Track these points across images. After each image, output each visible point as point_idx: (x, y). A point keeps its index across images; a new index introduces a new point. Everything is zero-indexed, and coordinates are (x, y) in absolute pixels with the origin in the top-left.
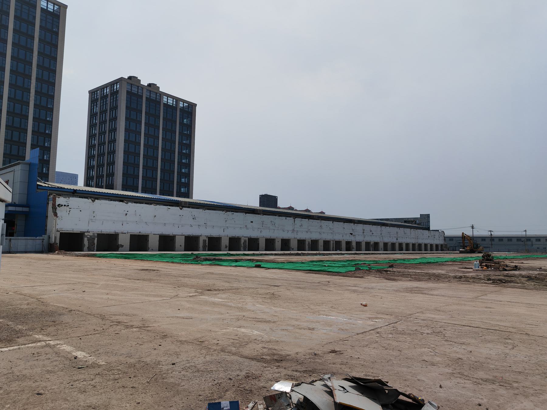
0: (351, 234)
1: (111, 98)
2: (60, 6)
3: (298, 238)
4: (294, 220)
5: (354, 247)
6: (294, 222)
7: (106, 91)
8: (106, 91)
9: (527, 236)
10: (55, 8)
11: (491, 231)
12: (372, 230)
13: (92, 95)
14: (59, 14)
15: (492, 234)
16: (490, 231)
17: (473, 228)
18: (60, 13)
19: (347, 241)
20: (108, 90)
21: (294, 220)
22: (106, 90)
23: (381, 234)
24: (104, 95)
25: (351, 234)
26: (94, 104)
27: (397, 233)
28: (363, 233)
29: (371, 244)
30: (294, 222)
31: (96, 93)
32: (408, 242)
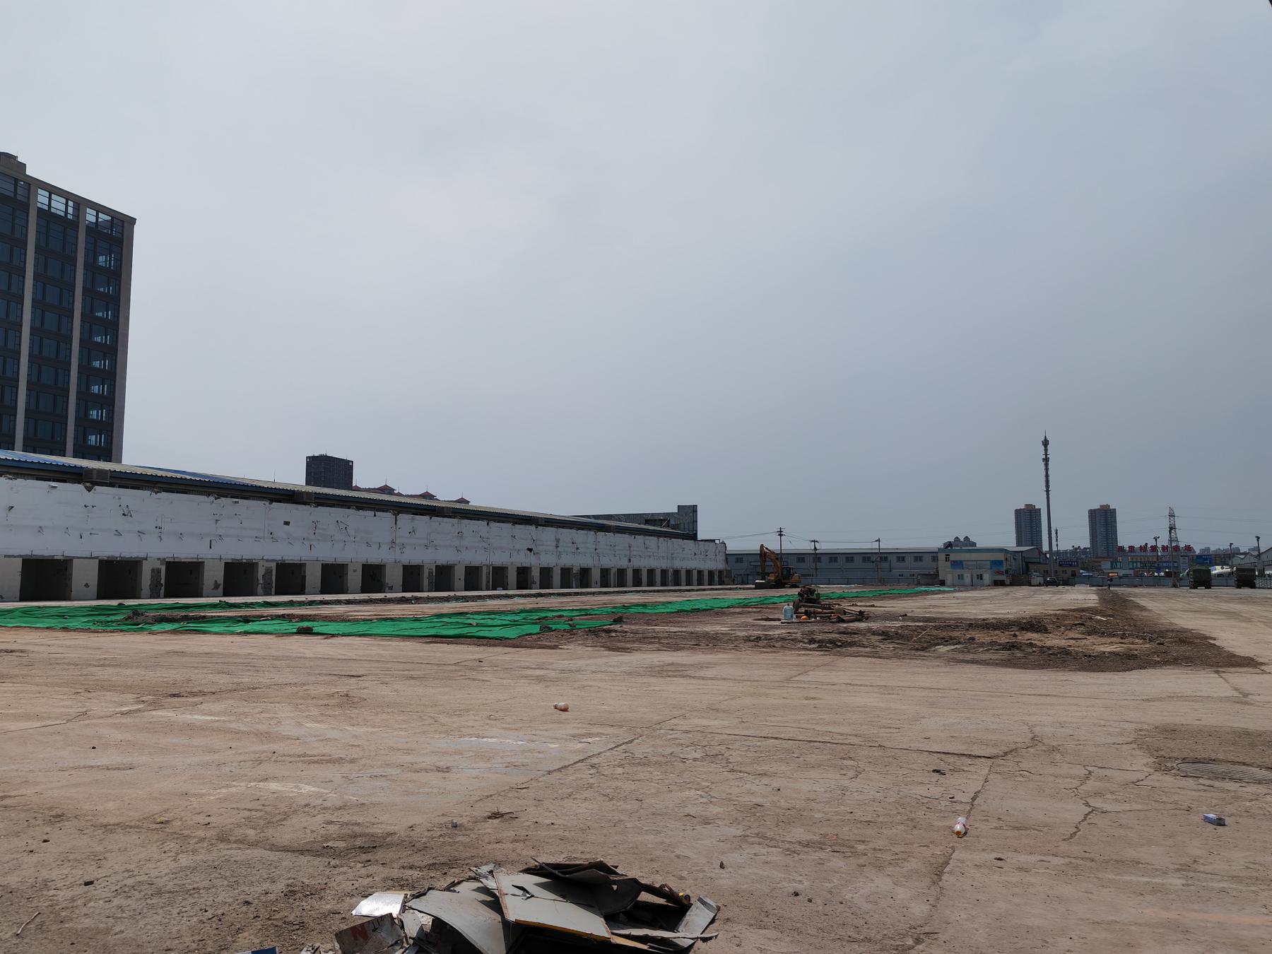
0: (530, 550)
3: (405, 562)
4: (396, 518)
5: (535, 580)
6: (396, 523)
9: (817, 552)
11: (814, 541)
12: (575, 540)
15: (817, 548)
16: (812, 541)
17: (781, 535)
19: (520, 566)
21: (396, 518)
23: (596, 549)
25: (530, 550)
27: (630, 547)
28: (557, 547)
29: (574, 572)
30: (396, 523)
32: (476, 563)
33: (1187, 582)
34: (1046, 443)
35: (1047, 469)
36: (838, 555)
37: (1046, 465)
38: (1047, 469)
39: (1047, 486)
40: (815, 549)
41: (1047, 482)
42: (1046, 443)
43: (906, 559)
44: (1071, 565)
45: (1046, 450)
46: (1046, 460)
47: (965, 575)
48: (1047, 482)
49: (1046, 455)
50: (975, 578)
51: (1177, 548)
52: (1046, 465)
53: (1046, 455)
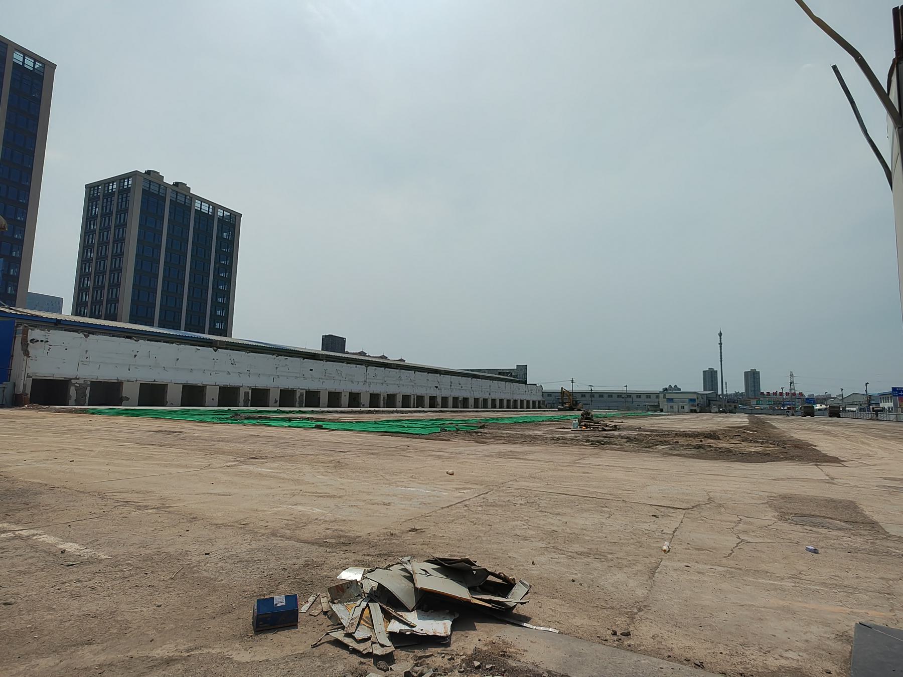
0: (437, 387)
1: (103, 201)
2: (45, 64)
7: (112, 187)
8: (112, 187)
10: (36, 66)
11: (591, 386)
13: (90, 191)
14: (42, 74)
17: (573, 382)
18: (44, 73)
20: (115, 186)
22: (113, 186)
24: (123, 187)
25: (437, 387)
26: (92, 204)
28: (451, 386)
31: (96, 188)
33: (800, 413)
34: (720, 334)
35: (721, 349)
36: (586, 394)
37: (721, 347)
38: (721, 349)
39: (721, 358)
40: (591, 390)
41: (721, 356)
42: (720, 334)
43: (642, 396)
44: (734, 402)
45: (721, 339)
46: (721, 344)
47: (674, 406)
48: (721, 356)
49: (721, 341)
50: (680, 408)
51: (794, 394)
52: (721, 347)
53: (721, 341)
